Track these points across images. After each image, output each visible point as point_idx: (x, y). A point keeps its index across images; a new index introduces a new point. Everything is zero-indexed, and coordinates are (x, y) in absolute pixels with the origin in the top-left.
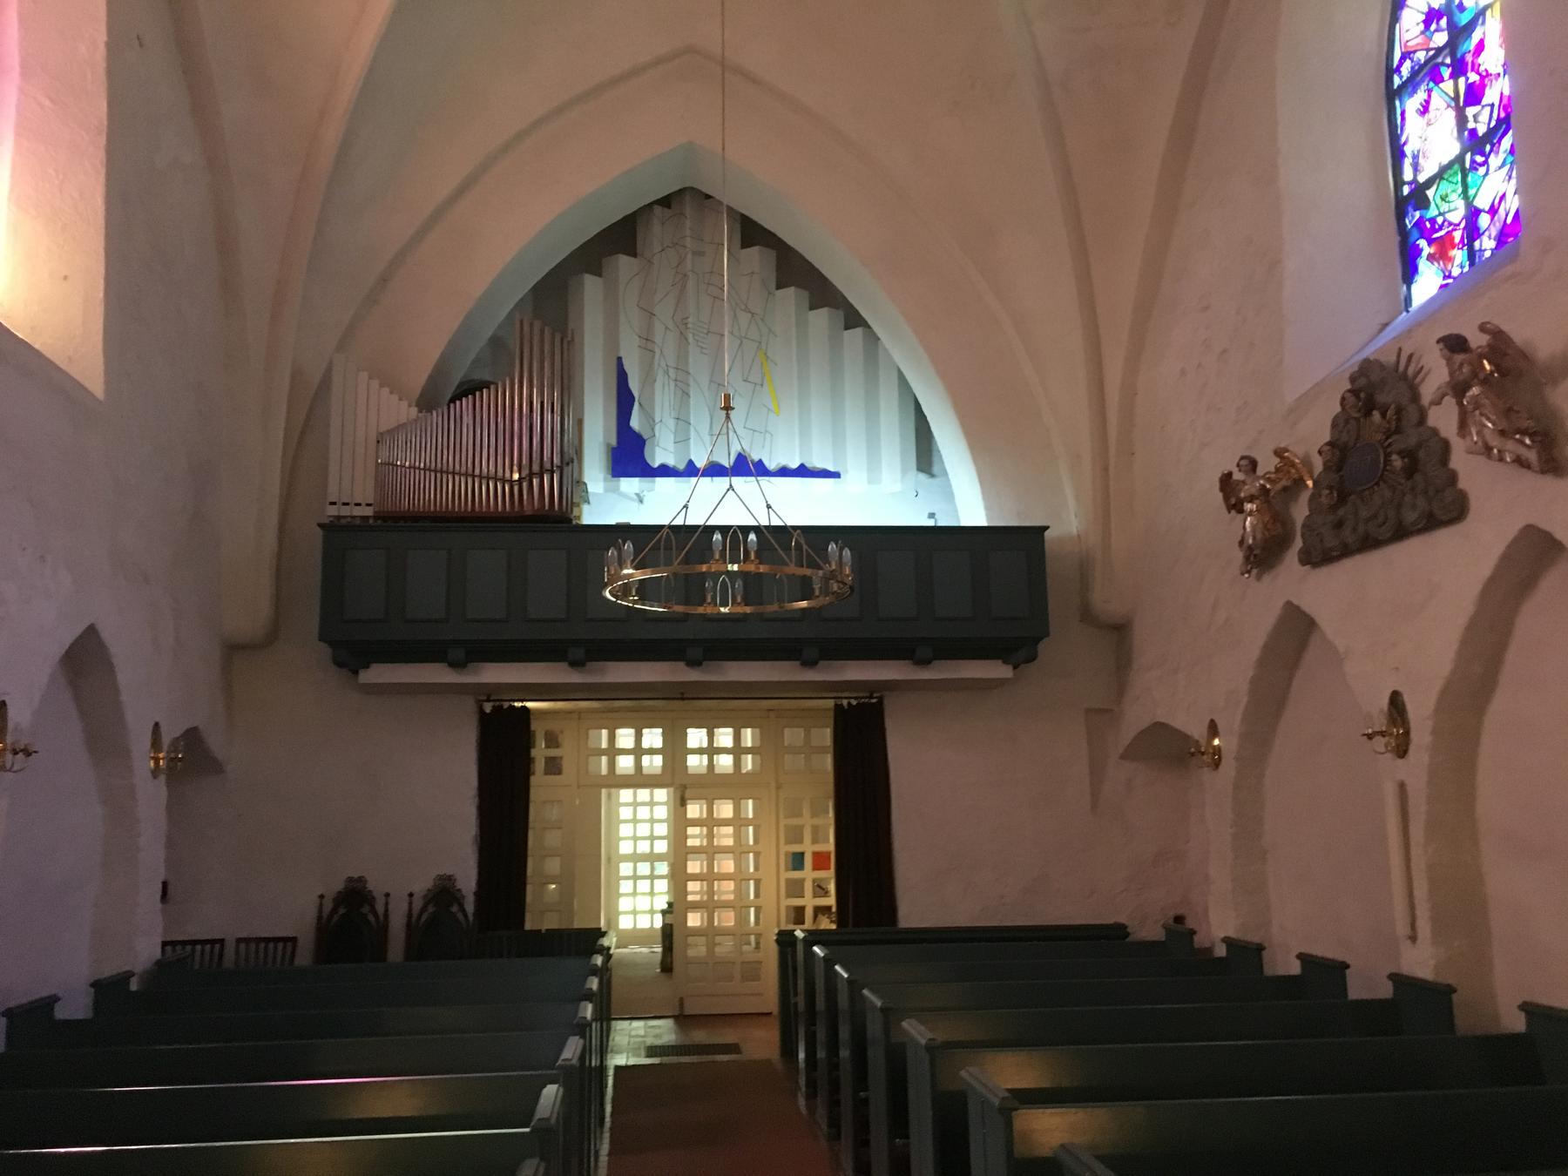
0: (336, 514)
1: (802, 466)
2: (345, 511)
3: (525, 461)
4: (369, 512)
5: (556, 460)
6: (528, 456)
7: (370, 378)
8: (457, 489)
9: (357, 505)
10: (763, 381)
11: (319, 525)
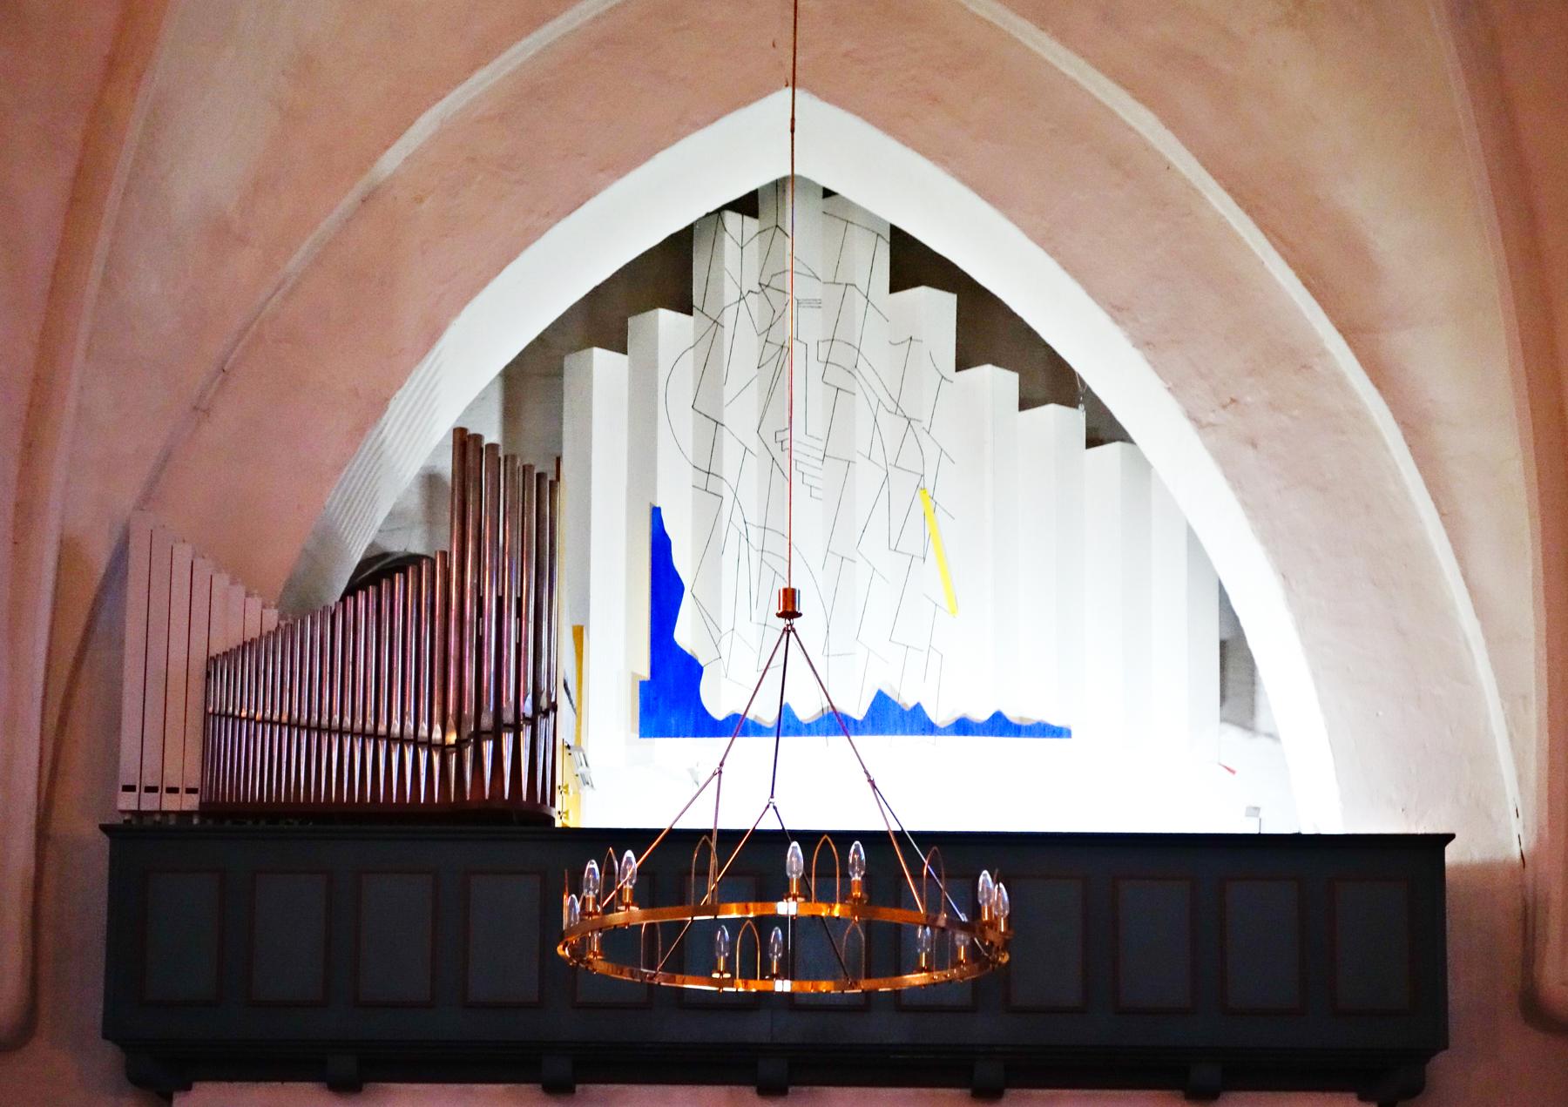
0: (135, 808)
1: (998, 716)
2: (150, 803)
3: (469, 710)
4: (191, 802)
5: (527, 708)
6: (442, 648)
7: (248, 594)
8: (346, 760)
9: (173, 790)
10: (926, 549)
11: (104, 828)
